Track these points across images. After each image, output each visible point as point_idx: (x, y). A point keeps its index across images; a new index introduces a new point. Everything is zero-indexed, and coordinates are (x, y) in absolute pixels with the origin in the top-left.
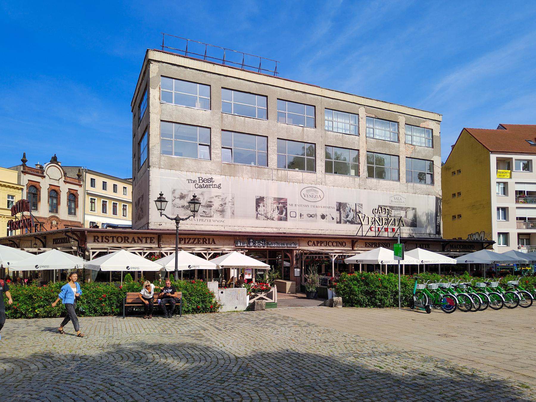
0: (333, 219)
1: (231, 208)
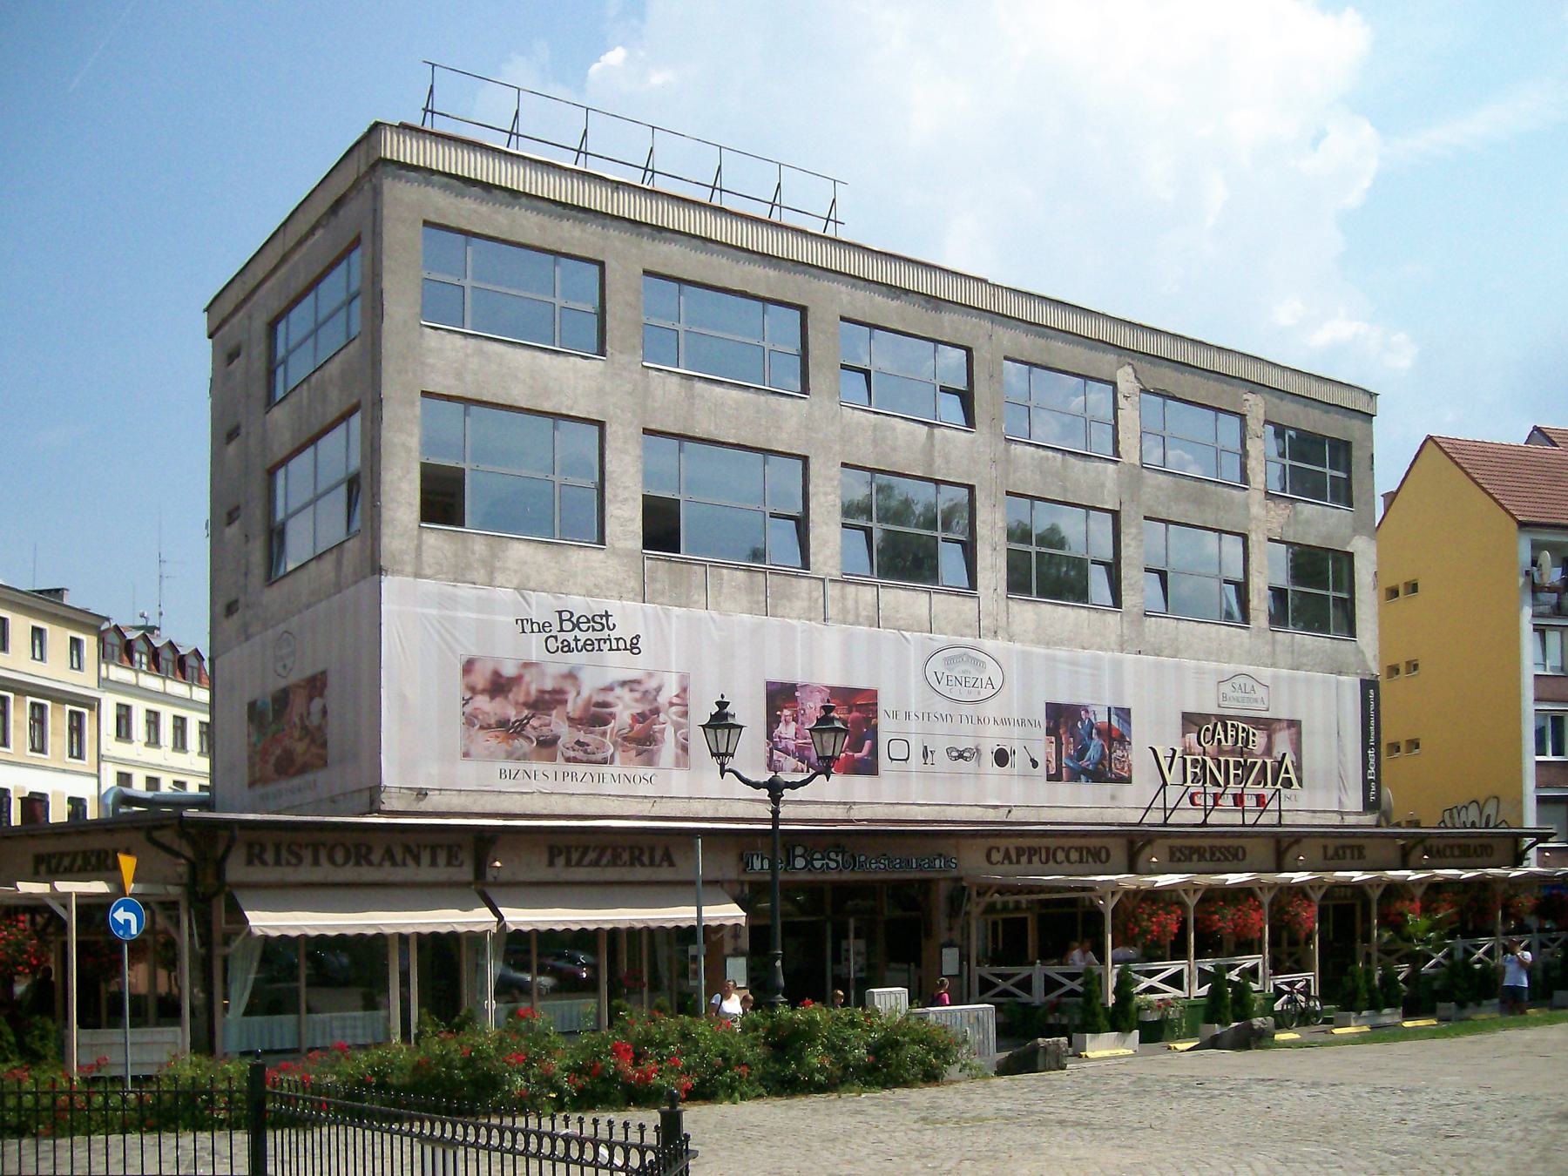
0: (1035, 764)
1: (678, 727)
